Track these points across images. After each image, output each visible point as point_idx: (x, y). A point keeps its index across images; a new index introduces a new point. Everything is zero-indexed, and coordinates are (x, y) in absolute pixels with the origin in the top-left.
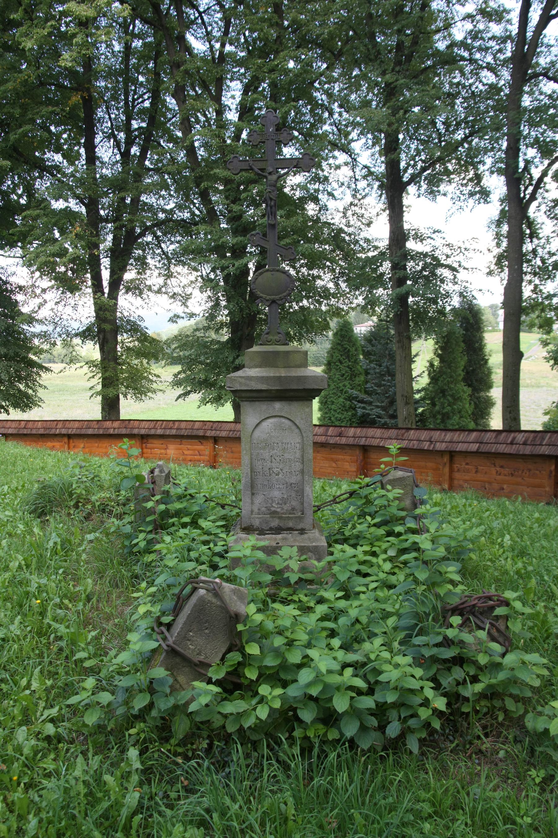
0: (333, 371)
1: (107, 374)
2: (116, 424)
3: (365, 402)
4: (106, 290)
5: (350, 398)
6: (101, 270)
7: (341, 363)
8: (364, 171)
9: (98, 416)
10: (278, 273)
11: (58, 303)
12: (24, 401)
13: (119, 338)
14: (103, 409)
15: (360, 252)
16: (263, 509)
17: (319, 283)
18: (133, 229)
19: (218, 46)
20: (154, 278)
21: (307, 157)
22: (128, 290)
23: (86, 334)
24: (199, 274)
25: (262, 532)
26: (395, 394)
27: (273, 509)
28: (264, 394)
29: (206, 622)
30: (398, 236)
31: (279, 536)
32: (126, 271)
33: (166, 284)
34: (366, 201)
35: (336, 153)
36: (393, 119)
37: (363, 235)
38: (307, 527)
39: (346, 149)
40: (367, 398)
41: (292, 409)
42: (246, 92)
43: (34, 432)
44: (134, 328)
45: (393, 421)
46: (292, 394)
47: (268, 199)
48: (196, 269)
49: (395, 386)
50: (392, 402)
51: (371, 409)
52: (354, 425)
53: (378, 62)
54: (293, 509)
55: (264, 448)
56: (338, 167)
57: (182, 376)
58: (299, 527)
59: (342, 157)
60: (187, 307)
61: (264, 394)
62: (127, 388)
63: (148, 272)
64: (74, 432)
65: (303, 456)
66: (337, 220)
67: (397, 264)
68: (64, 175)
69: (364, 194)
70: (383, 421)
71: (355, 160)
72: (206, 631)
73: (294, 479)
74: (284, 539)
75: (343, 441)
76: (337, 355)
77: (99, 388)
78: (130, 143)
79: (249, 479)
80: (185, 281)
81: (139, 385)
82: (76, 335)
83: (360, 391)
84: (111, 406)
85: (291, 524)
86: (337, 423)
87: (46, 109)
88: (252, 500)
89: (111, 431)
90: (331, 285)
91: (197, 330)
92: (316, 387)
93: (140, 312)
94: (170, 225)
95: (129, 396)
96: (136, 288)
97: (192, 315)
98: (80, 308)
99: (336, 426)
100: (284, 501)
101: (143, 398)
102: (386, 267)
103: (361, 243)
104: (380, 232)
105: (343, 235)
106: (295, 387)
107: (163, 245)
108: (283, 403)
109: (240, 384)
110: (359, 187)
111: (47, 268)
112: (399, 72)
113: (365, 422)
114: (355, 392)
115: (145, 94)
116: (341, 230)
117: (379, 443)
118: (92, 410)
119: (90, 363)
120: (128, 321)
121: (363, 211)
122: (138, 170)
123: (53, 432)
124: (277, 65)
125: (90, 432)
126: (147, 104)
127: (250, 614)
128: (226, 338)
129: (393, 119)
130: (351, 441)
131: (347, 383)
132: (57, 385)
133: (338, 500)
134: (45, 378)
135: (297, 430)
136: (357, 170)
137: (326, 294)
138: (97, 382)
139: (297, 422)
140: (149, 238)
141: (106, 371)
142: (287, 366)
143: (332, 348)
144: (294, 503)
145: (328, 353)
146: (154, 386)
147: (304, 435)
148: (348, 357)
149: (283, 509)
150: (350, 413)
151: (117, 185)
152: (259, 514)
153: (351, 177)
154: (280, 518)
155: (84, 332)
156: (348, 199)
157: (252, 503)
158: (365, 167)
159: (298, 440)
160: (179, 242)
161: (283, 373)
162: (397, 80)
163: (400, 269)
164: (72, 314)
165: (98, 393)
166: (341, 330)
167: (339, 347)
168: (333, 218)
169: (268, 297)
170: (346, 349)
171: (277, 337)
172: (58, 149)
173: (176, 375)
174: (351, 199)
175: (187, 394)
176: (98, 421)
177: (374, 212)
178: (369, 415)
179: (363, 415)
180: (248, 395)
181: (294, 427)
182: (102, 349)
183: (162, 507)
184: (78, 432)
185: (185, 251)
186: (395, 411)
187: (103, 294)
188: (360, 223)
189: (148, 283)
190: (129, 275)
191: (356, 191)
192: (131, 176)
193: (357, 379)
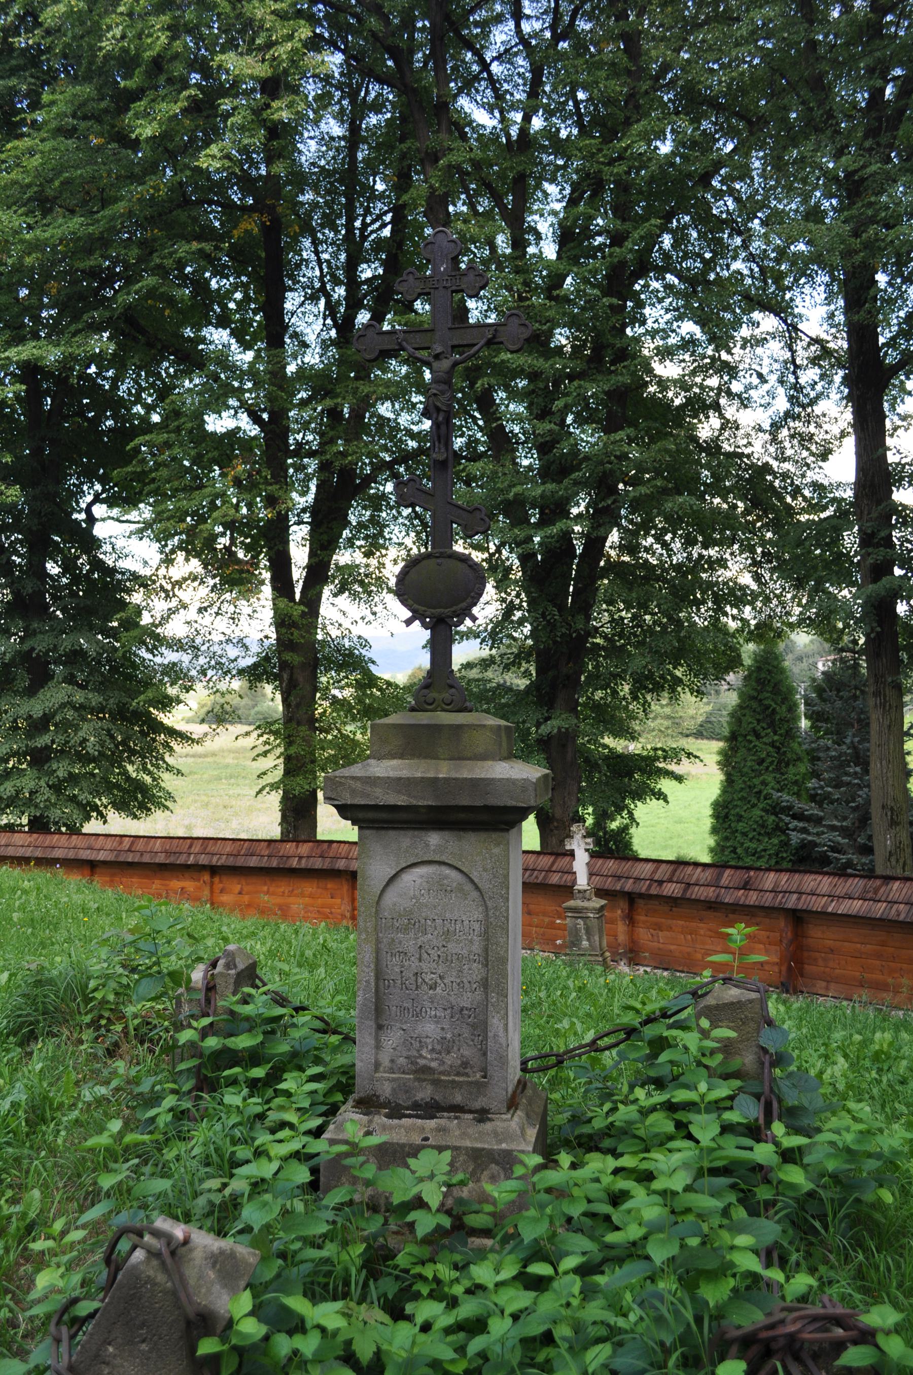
0: (742, 752)
1: (292, 750)
2: (304, 849)
3: (808, 819)
5: (776, 809)
7: (758, 736)
8: (813, 348)
9: (275, 832)
10: (449, 561)
11: (205, 609)
12: (138, 798)
14: (284, 817)
15: (803, 511)
16: (402, 1061)
17: (723, 575)
19: (518, 117)
21: (515, 320)
25: (396, 1112)
26: (868, 802)
27: (422, 1062)
28: (404, 816)
29: (143, 1325)
30: (876, 475)
31: (432, 1123)
34: (818, 409)
35: (756, 315)
36: (856, 243)
37: (811, 476)
38: (494, 1105)
39: (781, 309)
40: (812, 809)
41: (472, 850)
42: (572, 202)
43: (146, 859)
44: (351, 661)
45: (864, 860)
46: (462, 816)
49: (868, 786)
50: (864, 820)
51: (818, 834)
52: (785, 865)
53: (829, 132)
54: (465, 1064)
55: (405, 930)
56: (760, 342)
58: (477, 1105)
59: (768, 322)
61: (404, 816)
64: (223, 861)
65: (486, 950)
66: (759, 450)
67: (873, 535)
68: (231, 368)
69: (813, 394)
70: (843, 858)
71: (796, 330)
72: (144, 1347)
73: (467, 1000)
74: (441, 1130)
75: (753, 898)
76: (750, 720)
77: (279, 773)
78: (354, 304)
79: (371, 995)
83: (798, 794)
85: (458, 1098)
86: (749, 861)
87: (186, 247)
89: (294, 863)
90: (746, 579)
92: (511, 803)
93: (359, 630)
99: (736, 868)
100: (446, 1046)
102: (850, 540)
103: (807, 493)
104: (841, 469)
105: (769, 478)
106: (465, 802)
108: (447, 834)
109: (353, 792)
110: (802, 381)
111: (198, 545)
112: (870, 150)
113: (807, 860)
114: (786, 798)
115: (386, 213)
117: (826, 905)
118: (261, 818)
119: (266, 726)
121: (812, 428)
123: (181, 860)
124: (626, 149)
125: (253, 862)
126: (387, 232)
127: (236, 1317)
128: (522, 683)
129: (856, 243)
130: (768, 900)
131: (769, 778)
132: (227, 766)
134: (180, 755)
135: (475, 894)
136: (799, 346)
138: (273, 765)
139: (475, 876)
142: (459, 757)
143: (740, 707)
144: (467, 1052)
145: (732, 715)
147: (489, 904)
148: (772, 725)
149: (442, 1063)
150: (775, 841)
151: (321, 383)
153: (786, 362)
154: (436, 1083)
156: (782, 404)
157: (378, 1047)
159: (478, 914)
161: (444, 770)
162: (864, 167)
163: (878, 545)
164: (228, 632)
165: (274, 787)
166: (759, 669)
167: (754, 704)
168: (750, 444)
170: (767, 707)
171: (446, 695)
172: (223, 322)
176: (270, 842)
177: (836, 430)
178: (815, 844)
179: (804, 845)
181: (468, 887)
183: (212, 1042)
184: (231, 862)
186: (870, 838)
188: (805, 454)
190: (343, 557)
191: (797, 387)
193: (792, 769)
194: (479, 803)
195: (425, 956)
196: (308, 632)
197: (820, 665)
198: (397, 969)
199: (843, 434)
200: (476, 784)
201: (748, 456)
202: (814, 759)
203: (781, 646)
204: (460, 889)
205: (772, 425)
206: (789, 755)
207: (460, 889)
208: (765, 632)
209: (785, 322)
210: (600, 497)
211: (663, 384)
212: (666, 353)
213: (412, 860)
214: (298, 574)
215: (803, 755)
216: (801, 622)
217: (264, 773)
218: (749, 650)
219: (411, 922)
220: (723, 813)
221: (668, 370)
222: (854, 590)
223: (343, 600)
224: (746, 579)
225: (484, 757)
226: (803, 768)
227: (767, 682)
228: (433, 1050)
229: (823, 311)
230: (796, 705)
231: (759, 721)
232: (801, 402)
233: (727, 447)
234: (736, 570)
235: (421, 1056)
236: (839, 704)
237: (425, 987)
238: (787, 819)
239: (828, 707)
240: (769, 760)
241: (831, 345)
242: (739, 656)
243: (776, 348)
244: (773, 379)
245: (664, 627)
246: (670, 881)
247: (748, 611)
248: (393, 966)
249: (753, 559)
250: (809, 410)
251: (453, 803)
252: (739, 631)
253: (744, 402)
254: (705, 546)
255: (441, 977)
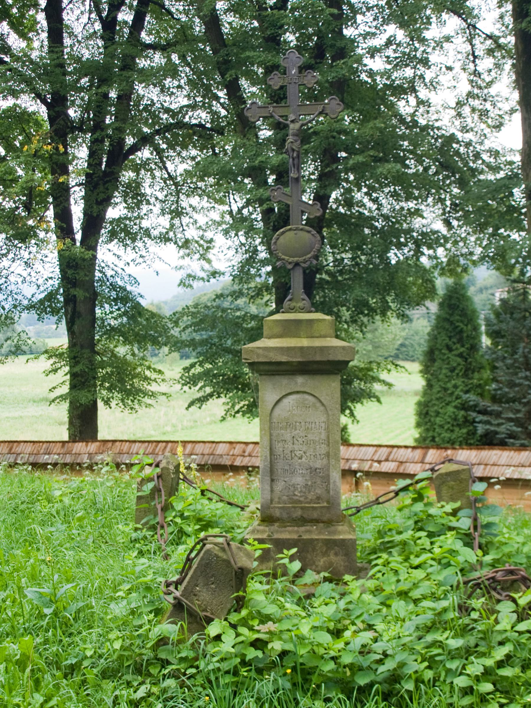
1: (77, 369)
2: (92, 447)
4: (78, 237)
5: (465, 407)
6: (69, 204)
7: (450, 349)
13: (98, 311)
16: (285, 498)
17: (417, 223)
18: (122, 142)
20: (155, 220)
22: (113, 235)
23: (43, 307)
24: (226, 208)
31: (303, 529)
32: (110, 204)
33: (172, 226)
34: (493, 91)
37: (488, 144)
40: (496, 408)
46: (315, 366)
47: (290, 150)
48: (221, 202)
51: (499, 425)
57: (198, 369)
59: (453, 23)
60: (209, 261)
62: (109, 389)
63: (145, 208)
65: (328, 437)
66: (447, 123)
69: (488, 79)
71: (475, 27)
72: (213, 586)
76: (443, 339)
77: (65, 389)
80: (202, 220)
81: (128, 385)
82: (31, 307)
83: (481, 395)
84: (83, 422)
88: (272, 487)
90: (439, 226)
91: (219, 296)
93: (131, 270)
94: (178, 132)
95: (113, 403)
96: (124, 233)
97: (214, 274)
98: (38, 266)
101: (137, 407)
106: (318, 358)
107: (169, 164)
108: (306, 377)
109: (258, 356)
114: (472, 398)
116: (452, 138)
120: (113, 287)
121: (488, 106)
122: (130, 50)
133: (381, 500)
135: (322, 408)
136: (477, 41)
137: (430, 239)
140: (146, 153)
141: (77, 363)
144: (319, 491)
146: (154, 387)
147: (330, 413)
148: (460, 341)
150: (464, 431)
152: (279, 503)
155: (41, 302)
156: (464, 87)
157: (272, 491)
158: (490, 37)
160: (193, 158)
161: (305, 342)
165: (62, 398)
167: (447, 326)
169: (291, 260)
173: (187, 369)
174: (469, 88)
175: (202, 400)
176: (64, 443)
177: (506, 107)
178: (496, 433)
180: (266, 368)
181: (318, 405)
182: (70, 330)
185: (202, 171)
187: (74, 240)
188: (483, 126)
189: (145, 224)
190: (113, 213)
191: (477, 73)
192: (119, 64)
194: (325, 359)
195: (296, 442)
196: (90, 272)
197: (497, 295)
198: (281, 449)
199: (512, 111)
200: (322, 349)
201: (438, 128)
202: (494, 368)
203: (466, 278)
204: (314, 405)
205: (457, 104)
206: (474, 364)
207: (314, 405)
208: (452, 267)
209: (465, 21)
210: (325, 165)
211: (371, 74)
212: (373, 52)
213: (289, 391)
214: (77, 224)
215: (485, 363)
216: (482, 259)
217: (54, 388)
218: (441, 283)
219: (289, 425)
220: (425, 414)
221: (377, 64)
222: (523, 234)
223: (114, 245)
224: (439, 226)
225: (325, 336)
226: (487, 374)
227: (456, 308)
228: (301, 492)
229: (497, 13)
230: (479, 325)
231: (450, 338)
232: (479, 86)
233: (422, 122)
234: (430, 218)
235: (295, 495)
236: (512, 323)
237: (296, 458)
238: (474, 414)
239: (504, 326)
240: (459, 368)
241: (502, 41)
242: (434, 286)
243: (460, 44)
244: (457, 66)
245: (376, 266)
246: (387, 460)
247: (440, 251)
248: (279, 448)
249: (444, 209)
250: (486, 91)
251: (311, 359)
252: (435, 267)
253: (433, 86)
254: (407, 200)
255: (305, 453)
